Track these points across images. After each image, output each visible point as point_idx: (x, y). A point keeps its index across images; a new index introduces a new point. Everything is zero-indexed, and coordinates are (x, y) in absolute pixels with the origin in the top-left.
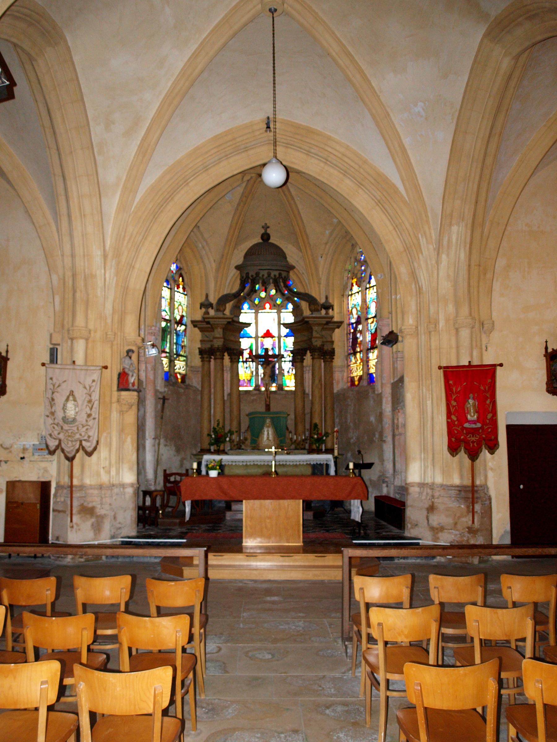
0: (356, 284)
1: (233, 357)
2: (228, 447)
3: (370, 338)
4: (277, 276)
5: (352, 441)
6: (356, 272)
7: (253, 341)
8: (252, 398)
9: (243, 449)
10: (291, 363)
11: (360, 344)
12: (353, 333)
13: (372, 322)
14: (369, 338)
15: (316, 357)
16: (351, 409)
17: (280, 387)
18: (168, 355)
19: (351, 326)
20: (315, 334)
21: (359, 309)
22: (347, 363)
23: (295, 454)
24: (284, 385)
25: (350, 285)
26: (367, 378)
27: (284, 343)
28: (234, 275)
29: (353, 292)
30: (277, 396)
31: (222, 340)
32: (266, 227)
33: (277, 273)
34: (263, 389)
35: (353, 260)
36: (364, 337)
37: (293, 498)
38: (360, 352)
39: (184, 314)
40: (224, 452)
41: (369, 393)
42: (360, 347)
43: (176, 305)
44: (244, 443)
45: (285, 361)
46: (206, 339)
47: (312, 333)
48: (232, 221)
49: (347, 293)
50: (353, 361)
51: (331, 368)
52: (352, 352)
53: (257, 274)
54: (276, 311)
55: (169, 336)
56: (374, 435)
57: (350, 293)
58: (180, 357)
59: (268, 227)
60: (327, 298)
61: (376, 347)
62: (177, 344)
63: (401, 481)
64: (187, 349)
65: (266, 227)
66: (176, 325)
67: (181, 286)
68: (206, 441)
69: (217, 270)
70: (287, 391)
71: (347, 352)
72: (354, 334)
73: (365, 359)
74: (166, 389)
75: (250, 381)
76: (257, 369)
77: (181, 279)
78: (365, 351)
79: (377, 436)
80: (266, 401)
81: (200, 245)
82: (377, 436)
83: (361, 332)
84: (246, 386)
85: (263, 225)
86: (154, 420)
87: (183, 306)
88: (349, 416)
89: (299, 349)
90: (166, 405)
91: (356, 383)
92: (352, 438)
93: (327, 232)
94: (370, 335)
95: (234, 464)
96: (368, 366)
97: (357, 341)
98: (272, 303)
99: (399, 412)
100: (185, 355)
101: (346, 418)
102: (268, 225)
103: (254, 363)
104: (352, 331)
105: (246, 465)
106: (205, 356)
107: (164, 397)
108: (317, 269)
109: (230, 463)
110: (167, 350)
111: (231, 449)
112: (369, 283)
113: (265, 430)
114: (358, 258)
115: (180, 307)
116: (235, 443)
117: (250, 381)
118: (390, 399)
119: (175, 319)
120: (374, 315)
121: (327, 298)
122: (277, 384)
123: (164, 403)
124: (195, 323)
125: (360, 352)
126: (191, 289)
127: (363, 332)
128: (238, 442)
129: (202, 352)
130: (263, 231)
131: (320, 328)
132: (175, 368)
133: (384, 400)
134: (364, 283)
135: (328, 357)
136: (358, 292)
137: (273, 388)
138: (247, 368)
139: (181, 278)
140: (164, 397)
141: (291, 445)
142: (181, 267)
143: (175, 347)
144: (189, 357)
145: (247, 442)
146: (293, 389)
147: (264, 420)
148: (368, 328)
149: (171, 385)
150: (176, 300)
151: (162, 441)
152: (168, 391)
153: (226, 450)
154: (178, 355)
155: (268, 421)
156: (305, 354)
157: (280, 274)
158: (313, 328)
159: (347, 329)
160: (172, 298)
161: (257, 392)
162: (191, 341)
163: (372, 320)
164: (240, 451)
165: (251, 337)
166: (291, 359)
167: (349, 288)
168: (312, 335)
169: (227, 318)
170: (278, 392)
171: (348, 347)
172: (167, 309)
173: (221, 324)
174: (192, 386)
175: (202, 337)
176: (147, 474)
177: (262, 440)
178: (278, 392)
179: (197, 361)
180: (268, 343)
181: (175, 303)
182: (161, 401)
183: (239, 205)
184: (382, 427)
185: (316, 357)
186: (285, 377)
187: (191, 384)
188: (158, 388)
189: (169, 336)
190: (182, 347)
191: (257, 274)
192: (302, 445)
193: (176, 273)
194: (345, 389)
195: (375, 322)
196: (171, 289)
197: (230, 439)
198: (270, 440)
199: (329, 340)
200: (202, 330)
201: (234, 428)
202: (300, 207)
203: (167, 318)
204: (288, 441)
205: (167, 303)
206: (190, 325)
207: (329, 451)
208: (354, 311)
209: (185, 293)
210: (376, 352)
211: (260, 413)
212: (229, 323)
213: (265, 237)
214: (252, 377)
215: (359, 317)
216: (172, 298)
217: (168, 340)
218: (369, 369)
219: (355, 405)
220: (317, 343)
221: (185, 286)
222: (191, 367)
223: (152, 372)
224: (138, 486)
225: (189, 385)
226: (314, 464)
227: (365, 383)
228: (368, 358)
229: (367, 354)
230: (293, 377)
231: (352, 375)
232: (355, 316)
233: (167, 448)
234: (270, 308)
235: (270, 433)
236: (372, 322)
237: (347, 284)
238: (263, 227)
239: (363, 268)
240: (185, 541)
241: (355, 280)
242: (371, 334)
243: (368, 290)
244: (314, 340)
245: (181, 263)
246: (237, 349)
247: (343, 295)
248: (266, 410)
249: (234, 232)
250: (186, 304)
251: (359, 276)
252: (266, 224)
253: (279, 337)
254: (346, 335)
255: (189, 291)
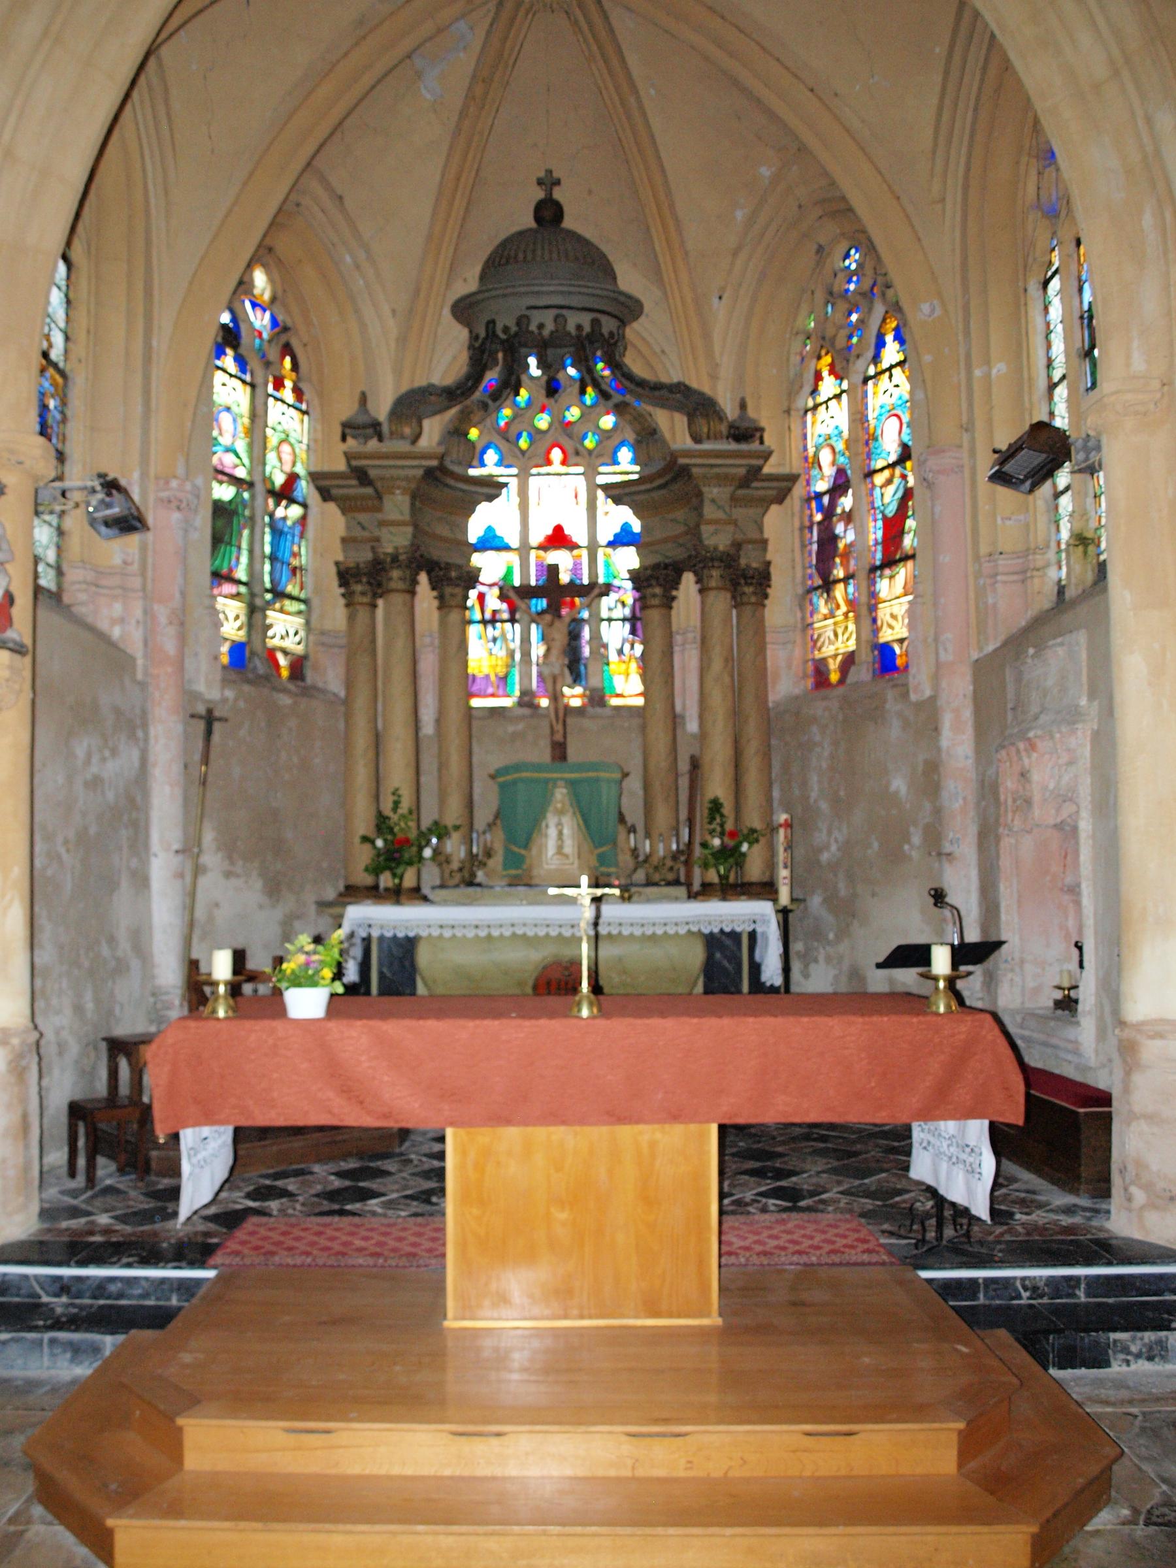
0: (831, 372)
1: (448, 590)
2: (430, 875)
3: (880, 534)
4: (587, 329)
5: (825, 857)
6: (830, 332)
7: (513, 558)
8: (511, 729)
9: (479, 885)
10: (628, 626)
11: (846, 556)
12: (819, 523)
13: (889, 482)
14: (875, 532)
15: (713, 583)
16: (822, 757)
17: (597, 698)
18: (243, 589)
19: (814, 505)
20: (709, 511)
21: (840, 446)
22: (803, 619)
23: (649, 900)
24: (607, 692)
25: (809, 377)
26: (870, 659)
27: (607, 565)
28: (455, 358)
29: (821, 399)
30: (586, 723)
31: (409, 530)
32: (549, 182)
33: (585, 320)
34: (544, 702)
35: (820, 296)
36: (861, 533)
37: (675, 1116)
38: (846, 580)
39: (300, 469)
40: (417, 895)
41: (885, 702)
42: (845, 565)
43: (273, 439)
44: (483, 865)
45: (610, 620)
46: (358, 533)
47: (698, 509)
48: (443, 176)
49: (800, 404)
50: (824, 609)
51: (760, 630)
52: (818, 582)
53: (523, 321)
54: (581, 469)
55: (246, 533)
56: (906, 838)
57: (810, 403)
58: (287, 602)
59: (558, 182)
60: (743, 406)
61: (906, 558)
62: (273, 558)
63: (1023, 994)
64: (309, 580)
65: (549, 182)
66: (271, 502)
67: (289, 384)
68: (363, 856)
69: (402, 340)
70: (618, 708)
71: (803, 583)
72: (826, 527)
73: (864, 599)
74: (229, 694)
75: (504, 679)
76: (526, 640)
77: (287, 362)
78: (862, 575)
79: (916, 839)
80: (553, 732)
81: (348, 259)
82: (916, 839)
83: (848, 517)
84: (493, 695)
85: (542, 174)
86: (178, 792)
87: (297, 446)
88: (814, 778)
89: (656, 567)
90: (216, 738)
91: (834, 677)
92: (827, 847)
93: (739, 215)
94: (880, 524)
95: (447, 933)
96: (874, 620)
97: (836, 547)
98: (569, 445)
99: (1032, 747)
100: (302, 596)
101: (804, 784)
102: (555, 175)
103: (517, 626)
104: (818, 517)
105: (489, 937)
106: (358, 588)
107: (210, 712)
108: (707, 336)
109: (436, 932)
110: (241, 574)
111: (442, 886)
112: (876, 359)
113: (551, 820)
114: (836, 289)
115: (286, 448)
116: (455, 865)
117: (504, 679)
118: (967, 714)
119: (268, 480)
120: (893, 458)
121: (743, 406)
122: (585, 689)
123: (209, 732)
124: (324, 485)
125: (846, 580)
126: (321, 395)
127: (855, 515)
128: (462, 862)
129: (345, 576)
130: (540, 194)
131: (728, 490)
132: (270, 633)
133: (947, 721)
134: (860, 364)
135: (748, 590)
136: (837, 397)
137: (574, 696)
138: (495, 640)
139: (288, 360)
140: (210, 712)
141: (635, 870)
142: (289, 324)
143: (267, 567)
144: (315, 602)
145: (491, 863)
146: (640, 702)
147: (546, 788)
148: (873, 503)
149: (249, 682)
150: (270, 423)
151: (211, 859)
152: (236, 700)
153: (426, 890)
154: (279, 594)
155: (560, 794)
156: (675, 583)
157: (595, 323)
158: (705, 490)
159: (802, 512)
160: (257, 416)
161: (526, 711)
162: (318, 552)
163: (887, 473)
164: (471, 890)
165: (507, 548)
166: (627, 612)
167: (808, 388)
168: (701, 515)
169: (424, 456)
170: (590, 709)
171: (804, 568)
172: (241, 446)
173: (407, 479)
174: (323, 691)
175: (348, 528)
176: (156, 971)
177: (540, 853)
178: (590, 709)
179: (336, 614)
180: (561, 558)
181: (269, 431)
182: (201, 725)
183: (463, 114)
184: (938, 811)
185: (713, 583)
186: (612, 666)
187: (320, 685)
188: (201, 687)
189: (246, 533)
190: (294, 570)
191: (523, 321)
192: (671, 869)
193: (270, 341)
194: (797, 697)
195: (897, 480)
196: (253, 386)
197: (437, 852)
198: (567, 856)
199: (753, 534)
200: (347, 506)
201: (453, 814)
202: (656, 123)
203: (241, 473)
204: (626, 859)
205: (240, 429)
206: (314, 498)
207: (767, 890)
208: (825, 457)
209: (304, 407)
210: (902, 573)
211: (538, 767)
212: (429, 473)
213: (547, 214)
214: (510, 666)
215: (841, 472)
216: (257, 416)
217: (244, 545)
218: (876, 631)
219: (836, 744)
220: (717, 539)
221: (302, 385)
222: (323, 633)
223: (171, 631)
224: (36, 1035)
225: (314, 687)
226: (711, 934)
227: (862, 673)
228: (874, 595)
229: (873, 583)
230: (634, 666)
231: (818, 655)
232: (829, 471)
233: (235, 882)
234: (564, 463)
235: (566, 831)
236: (889, 482)
237: (800, 375)
238: (540, 182)
239: (854, 317)
240: (210, 1274)
241: (827, 360)
242: (885, 519)
243: (870, 383)
244: (706, 530)
245: (288, 312)
246: (459, 567)
247: (788, 412)
248: (554, 758)
249: (451, 204)
250: (305, 441)
251: (841, 342)
252: (549, 172)
253: (593, 548)
254: (797, 533)
255: (316, 402)
